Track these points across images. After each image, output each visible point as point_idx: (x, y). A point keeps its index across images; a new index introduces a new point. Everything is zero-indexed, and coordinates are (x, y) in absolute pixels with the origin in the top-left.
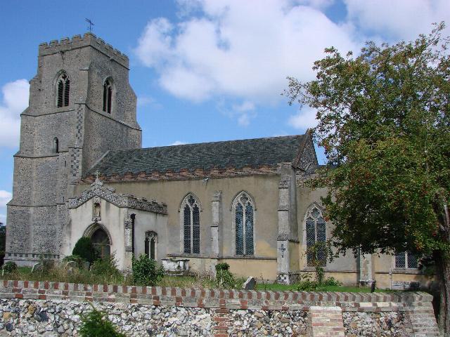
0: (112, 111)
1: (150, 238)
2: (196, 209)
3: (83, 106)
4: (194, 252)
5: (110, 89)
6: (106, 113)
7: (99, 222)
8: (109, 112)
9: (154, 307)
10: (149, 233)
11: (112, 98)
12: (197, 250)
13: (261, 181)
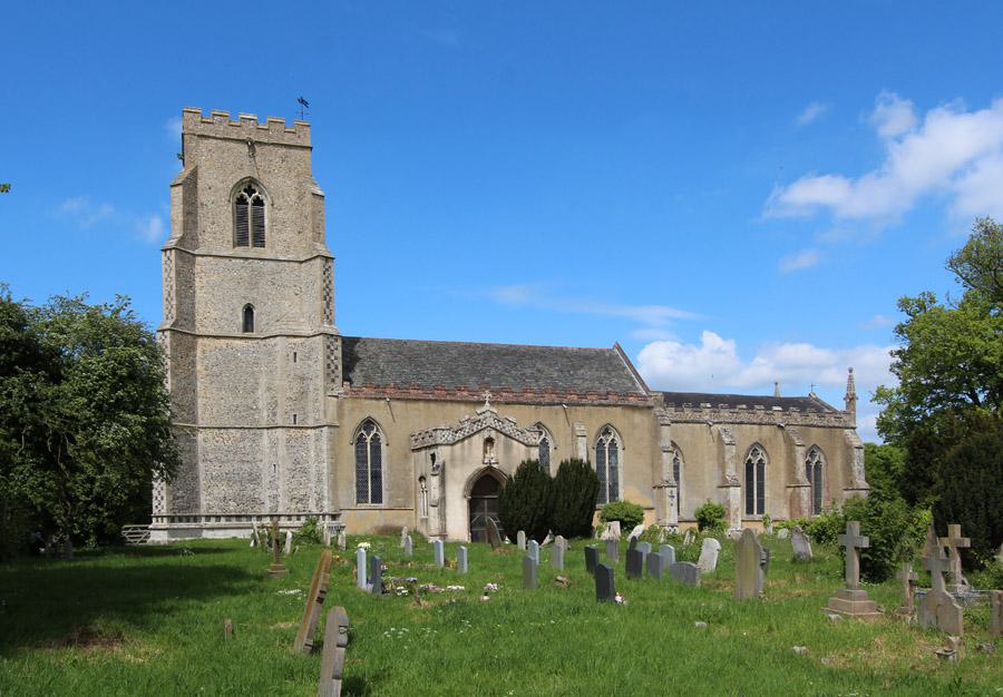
7: (495, 466)
13: (628, 413)
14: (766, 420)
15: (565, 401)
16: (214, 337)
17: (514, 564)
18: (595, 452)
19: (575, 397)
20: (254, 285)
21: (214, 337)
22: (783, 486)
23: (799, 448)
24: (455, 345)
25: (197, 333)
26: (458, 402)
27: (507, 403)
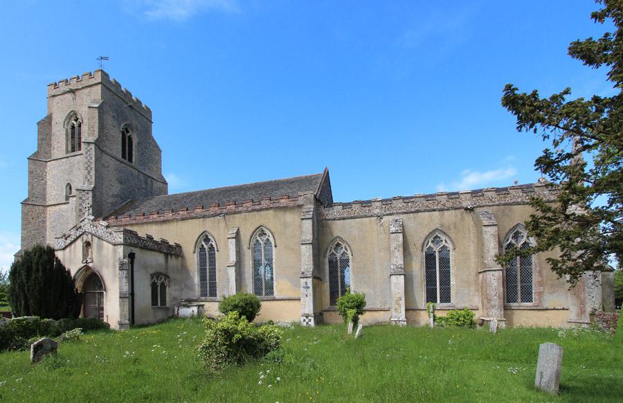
0: (134, 160)
1: (159, 283)
2: (212, 248)
3: (93, 146)
4: (211, 295)
5: (130, 138)
6: (129, 163)
7: (90, 265)
8: (130, 160)
9: (146, 377)
10: (157, 275)
11: (134, 153)
12: (527, 296)
13: (280, 214)
14: (449, 205)
15: (225, 211)
16: (54, 205)
17: (217, 364)
18: (250, 251)
19: (233, 207)
20: (70, 172)
21: (54, 205)
22: (473, 273)
23: (489, 229)
24: (199, 192)
25: (47, 204)
26: (150, 223)
27: (183, 219)
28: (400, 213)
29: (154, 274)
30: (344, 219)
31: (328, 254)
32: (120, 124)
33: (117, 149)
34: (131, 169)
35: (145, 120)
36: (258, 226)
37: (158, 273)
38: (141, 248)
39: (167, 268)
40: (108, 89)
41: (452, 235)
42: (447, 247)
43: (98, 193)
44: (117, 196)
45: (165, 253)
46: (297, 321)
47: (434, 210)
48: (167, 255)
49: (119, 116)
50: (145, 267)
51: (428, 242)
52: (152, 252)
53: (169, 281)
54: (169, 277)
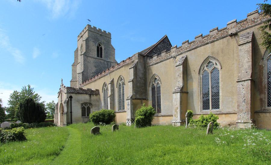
1: (86, 107)
5: (101, 48)
8: (101, 57)
28: (185, 52)
29: (83, 103)
30: (157, 63)
31: (151, 84)
32: (96, 44)
33: (95, 54)
34: (100, 60)
35: (108, 38)
36: (119, 76)
37: (85, 103)
38: (76, 93)
39: (90, 100)
40: (91, 31)
41: (220, 59)
42: (217, 68)
43: (85, 73)
44: (94, 73)
45: (89, 94)
46: (125, 122)
47: (207, 44)
48: (90, 95)
49: (96, 40)
50: (78, 101)
51: (204, 68)
52: (82, 95)
53: (92, 106)
54: (92, 104)
